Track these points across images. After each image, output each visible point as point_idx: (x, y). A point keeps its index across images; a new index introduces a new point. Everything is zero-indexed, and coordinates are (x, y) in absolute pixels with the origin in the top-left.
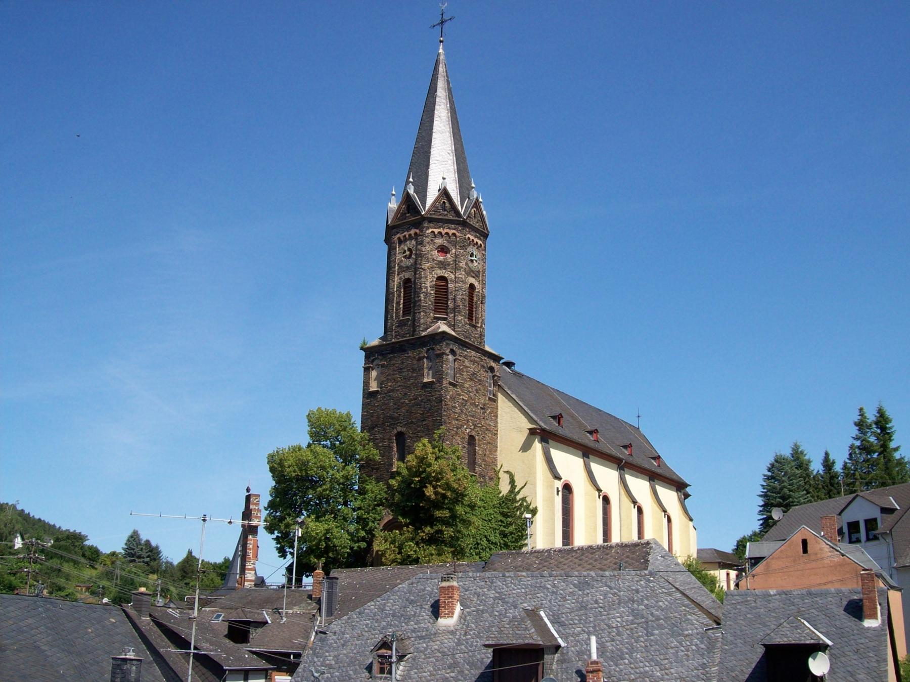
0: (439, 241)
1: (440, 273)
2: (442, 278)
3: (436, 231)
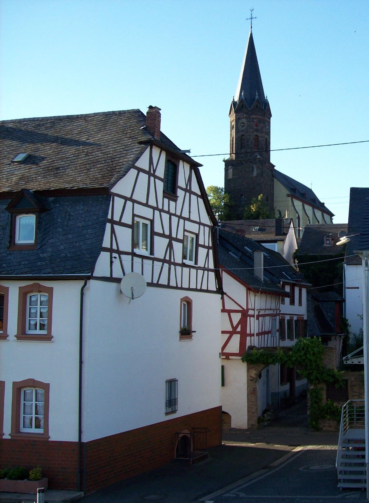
0: (255, 120)
1: (256, 133)
2: (257, 136)
3: (254, 116)
